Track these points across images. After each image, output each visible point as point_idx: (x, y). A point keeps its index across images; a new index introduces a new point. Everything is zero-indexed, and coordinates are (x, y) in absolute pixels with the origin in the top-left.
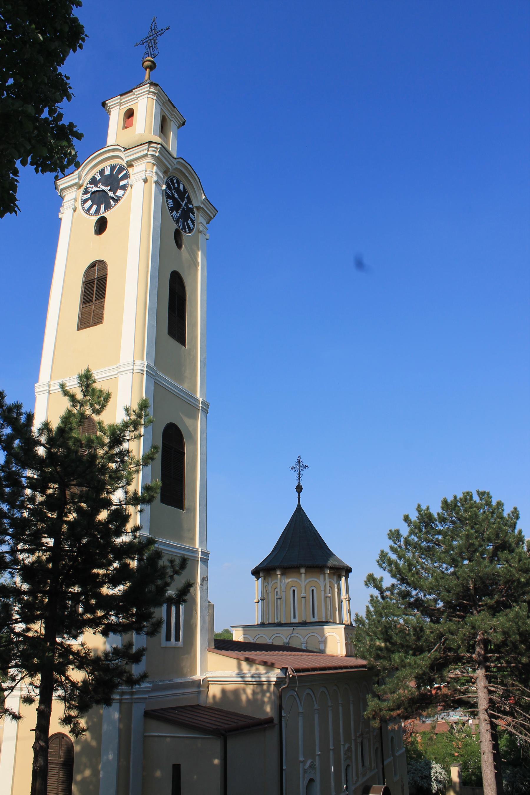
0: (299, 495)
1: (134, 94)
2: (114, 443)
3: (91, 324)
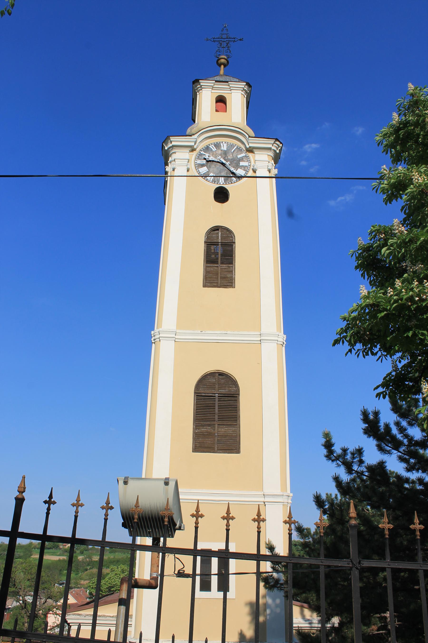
1: (229, 86)
3: (219, 285)
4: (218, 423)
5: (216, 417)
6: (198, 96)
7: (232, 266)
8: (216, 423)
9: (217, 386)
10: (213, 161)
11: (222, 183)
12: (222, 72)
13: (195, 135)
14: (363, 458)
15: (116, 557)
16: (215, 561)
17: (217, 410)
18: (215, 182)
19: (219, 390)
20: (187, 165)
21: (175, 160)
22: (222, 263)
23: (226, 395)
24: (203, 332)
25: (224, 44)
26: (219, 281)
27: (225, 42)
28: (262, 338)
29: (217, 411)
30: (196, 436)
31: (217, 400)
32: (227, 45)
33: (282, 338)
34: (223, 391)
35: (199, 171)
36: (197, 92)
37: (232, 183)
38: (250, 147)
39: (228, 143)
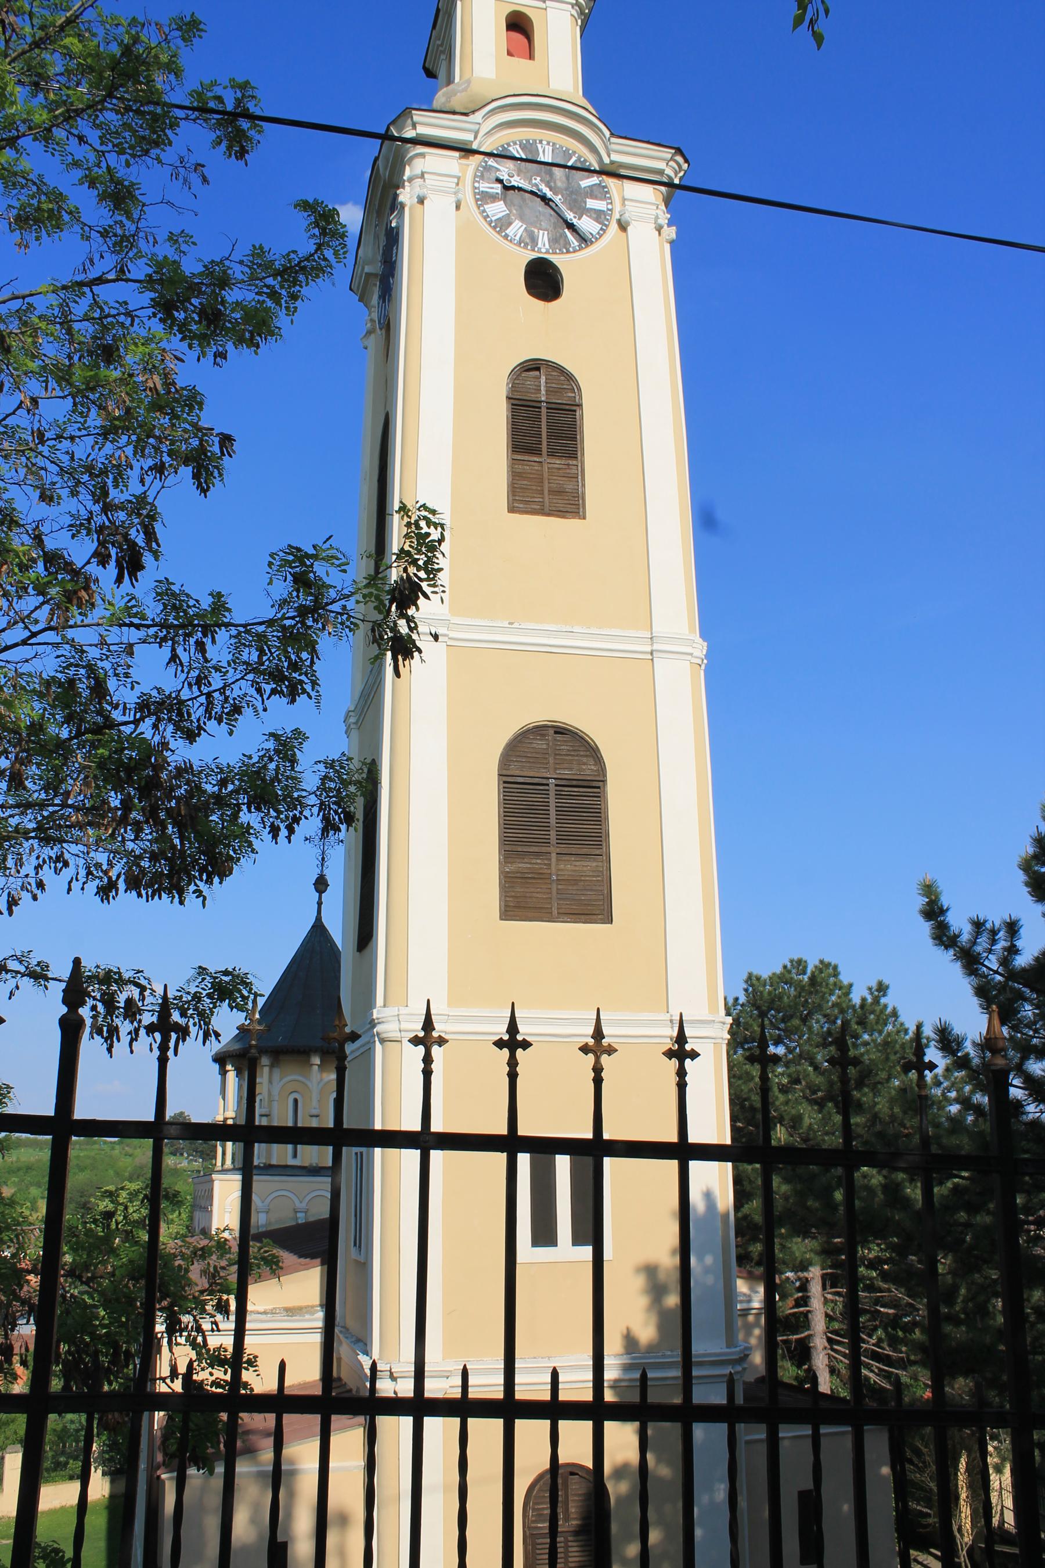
0: (320, 898)
2: (41, 725)
4: (558, 850)
5: (553, 834)
7: (575, 462)
8: (553, 850)
9: (551, 760)
10: (520, 189)
11: (543, 250)
13: (477, 114)
14: (1019, 944)
15: (23, 1159)
17: (554, 816)
18: (526, 245)
19: (556, 769)
20: (455, 193)
21: (423, 174)
22: (551, 454)
23: (574, 783)
24: (516, 625)
26: (547, 500)
28: (656, 647)
29: (553, 820)
30: (509, 882)
31: (552, 793)
33: (700, 648)
34: (566, 773)
35: (484, 211)
37: (568, 252)
38: (612, 163)
39: (554, 144)
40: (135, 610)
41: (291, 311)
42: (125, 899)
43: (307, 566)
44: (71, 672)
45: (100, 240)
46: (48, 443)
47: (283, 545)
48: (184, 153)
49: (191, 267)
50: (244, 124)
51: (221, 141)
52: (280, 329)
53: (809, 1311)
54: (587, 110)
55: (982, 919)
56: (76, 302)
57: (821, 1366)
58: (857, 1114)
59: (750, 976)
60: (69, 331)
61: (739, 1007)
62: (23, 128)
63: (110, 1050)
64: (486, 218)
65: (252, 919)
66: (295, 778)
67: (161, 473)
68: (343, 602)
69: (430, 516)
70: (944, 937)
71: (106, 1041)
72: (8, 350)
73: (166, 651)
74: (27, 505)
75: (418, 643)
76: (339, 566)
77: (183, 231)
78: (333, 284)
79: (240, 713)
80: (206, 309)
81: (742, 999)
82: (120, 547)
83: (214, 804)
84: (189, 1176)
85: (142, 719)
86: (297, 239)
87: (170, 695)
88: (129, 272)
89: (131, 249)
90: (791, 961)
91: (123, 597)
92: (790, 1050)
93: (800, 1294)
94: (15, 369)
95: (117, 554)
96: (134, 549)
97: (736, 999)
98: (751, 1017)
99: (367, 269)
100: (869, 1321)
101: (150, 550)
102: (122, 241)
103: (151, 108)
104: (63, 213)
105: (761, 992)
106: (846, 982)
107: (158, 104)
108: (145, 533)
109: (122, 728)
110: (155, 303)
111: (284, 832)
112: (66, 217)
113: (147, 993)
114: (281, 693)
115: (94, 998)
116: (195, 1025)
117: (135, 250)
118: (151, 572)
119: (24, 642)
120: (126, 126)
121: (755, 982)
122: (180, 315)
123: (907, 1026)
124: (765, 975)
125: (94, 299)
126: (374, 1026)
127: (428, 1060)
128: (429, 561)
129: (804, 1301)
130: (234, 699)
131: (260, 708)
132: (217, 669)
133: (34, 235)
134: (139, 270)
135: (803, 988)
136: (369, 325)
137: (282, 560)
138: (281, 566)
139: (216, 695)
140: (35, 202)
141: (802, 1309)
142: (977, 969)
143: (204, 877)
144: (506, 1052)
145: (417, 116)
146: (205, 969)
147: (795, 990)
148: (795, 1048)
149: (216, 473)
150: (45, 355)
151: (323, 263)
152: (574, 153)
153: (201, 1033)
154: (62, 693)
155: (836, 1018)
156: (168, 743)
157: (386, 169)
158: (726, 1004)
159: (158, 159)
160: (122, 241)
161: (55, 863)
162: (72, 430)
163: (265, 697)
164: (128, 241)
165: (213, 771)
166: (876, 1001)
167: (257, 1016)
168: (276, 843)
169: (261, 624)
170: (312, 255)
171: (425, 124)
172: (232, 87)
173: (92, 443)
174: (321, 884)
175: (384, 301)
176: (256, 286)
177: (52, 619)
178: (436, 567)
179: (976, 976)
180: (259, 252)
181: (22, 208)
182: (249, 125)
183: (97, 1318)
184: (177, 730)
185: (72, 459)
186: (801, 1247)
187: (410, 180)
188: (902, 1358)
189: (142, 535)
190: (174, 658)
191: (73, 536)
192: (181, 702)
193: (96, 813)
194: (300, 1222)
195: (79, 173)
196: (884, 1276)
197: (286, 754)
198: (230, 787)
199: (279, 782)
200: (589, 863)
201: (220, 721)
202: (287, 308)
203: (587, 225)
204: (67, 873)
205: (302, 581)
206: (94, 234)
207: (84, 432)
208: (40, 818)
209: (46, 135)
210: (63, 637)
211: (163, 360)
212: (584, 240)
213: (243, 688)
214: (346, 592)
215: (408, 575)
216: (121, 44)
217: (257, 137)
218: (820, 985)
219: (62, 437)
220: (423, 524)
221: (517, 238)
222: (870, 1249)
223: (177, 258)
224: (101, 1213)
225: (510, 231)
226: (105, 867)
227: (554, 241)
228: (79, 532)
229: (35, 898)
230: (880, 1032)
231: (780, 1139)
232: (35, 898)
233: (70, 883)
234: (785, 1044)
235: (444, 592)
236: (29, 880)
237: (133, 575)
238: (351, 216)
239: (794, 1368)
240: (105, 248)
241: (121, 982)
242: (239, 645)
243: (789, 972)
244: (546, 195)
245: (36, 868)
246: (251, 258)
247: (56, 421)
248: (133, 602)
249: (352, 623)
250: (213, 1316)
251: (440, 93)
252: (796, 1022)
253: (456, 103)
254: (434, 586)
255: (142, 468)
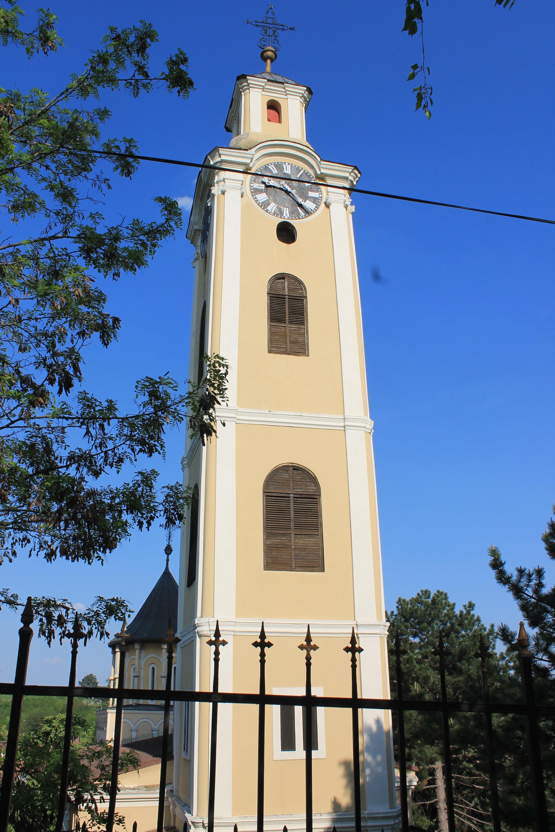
0: (168, 557)
1: (284, 89)
4: (295, 532)
5: (292, 524)
6: (243, 97)
7: (303, 327)
8: (292, 532)
10: (274, 187)
11: (286, 218)
12: (268, 69)
13: (252, 150)
14: (544, 581)
16: (298, 710)
17: (293, 514)
18: (277, 215)
19: (294, 489)
20: (241, 189)
21: (224, 179)
22: (291, 322)
23: (304, 496)
25: (270, 32)
26: (288, 347)
27: (271, 28)
28: (346, 423)
29: (292, 516)
30: (268, 549)
31: (292, 502)
32: (274, 34)
33: (370, 424)
34: (299, 491)
35: (256, 198)
36: (241, 92)
37: (299, 218)
38: (322, 174)
39: (292, 164)
40: (66, 410)
41: (152, 253)
42: (60, 560)
43: (156, 388)
44: (33, 440)
45: (55, 217)
46: (24, 321)
47: (144, 377)
48: (99, 173)
49: (101, 230)
50: (130, 160)
51: (118, 168)
52: (147, 261)
53: (436, 787)
54: (308, 147)
55: (523, 568)
56: (41, 249)
57: (444, 820)
58: (460, 675)
59: (400, 600)
60: (37, 264)
61: (394, 617)
62: (17, 163)
63: (49, 643)
64: (256, 201)
65: (129, 571)
66: (151, 496)
67: (83, 335)
68: (175, 406)
69: (221, 361)
70: (503, 578)
71: (47, 638)
72: (4, 276)
73: (84, 430)
74: (12, 352)
75: (215, 428)
76: (172, 388)
77: (97, 212)
78: (174, 239)
79: (123, 462)
80: (107, 251)
81: (396, 612)
82: (61, 375)
83: (108, 509)
84: (95, 710)
85: (71, 465)
86: (157, 216)
87: (85, 452)
88: (69, 232)
89: (71, 221)
90: (422, 591)
91: (59, 403)
92: (422, 640)
93: (431, 778)
94: (7, 284)
95: (59, 378)
96: (68, 376)
97: (392, 612)
98: (400, 622)
99: (195, 227)
100: (469, 793)
101: (77, 376)
102: (66, 217)
103: (83, 153)
104: (37, 203)
105: (406, 609)
106: (451, 603)
107: (85, 150)
108: (74, 368)
109: (60, 470)
110: (81, 249)
111: (145, 525)
112: (38, 206)
113: (70, 612)
114: (144, 451)
115: (41, 615)
116: (96, 628)
117: (73, 222)
118: (77, 387)
119: (8, 426)
120: (70, 161)
121: (402, 603)
122: (94, 255)
123: (485, 626)
124: (408, 599)
125: (51, 247)
126: (196, 628)
127: (217, 653)
128: (220, 384)
129: (433, 782)
130: (119, 454)
131: (133, 459)
132: (111, 438)
133: (21, 215)
134: (74, 232)
135: (428, 606)
136: (196, 256)
137: (143, 385)
138: (142, 388)
139: (110, 452)
140: (22, 198)
141: (432, 786)
142: (521, 596)
143: (102, 549)
144: (259, 649)
145: (221, 151)
146: (102, 598)
147: (424, 607)
148: (425, 639)
149: (112, 336)
150: (25, 275)
151: (169, 228)
152: (302, 169)
153: (99, 633)
154: (29, 451)
155: (447, 622)
156: (84, 478)
157: (205, 177)
158: (386, 615)
159: (86, 177)
160: (66, 217)
161: (22, 542)
162: (36, 315)
163: (136, 453)
164: (69, 217)
165: (107, 492)
166: (468, 612)
167: (126, 629)
168: (141, 531)
169: (131, 417)
170: (164, 224)
171: (226, 155)
172: (124, 141)
173: (46, 322)
174: (168, 550)
175: (204, 244)
176: (135, 240)
177: (22, 414)
178: (224, 387)
179: (521, 599)
180: (136, 222)
181: (16, 201)
182: (132, 160)
183: (36, 796)
184: (89, 471)
185: (36, 329)
186: (430, 751)
187: (218, 182)
188: (489, 815)
189: (72, 369)
190: (88, 433)
191: (36, 368)
192: (92, 456)
193: (44, 515)
194: (155, 736)
195: (45, 184)
196: (477, 767)
197: (147, 483)
198: (117, 501)
199: (143, 498)
200: (312, 539)
201: (112, 466)
202: (150, 251)
203: (309, 205)
204: (29, 546)
205: (154, 395)
206: (52, 214)
207: (43, 316)
208: (16, 516)
209: (28, 166)
210: (28, 424)
211: (83, 281)
212: (308, 212)
213: (124, 449)
214: (176, 401)
215: (209, 393)
216: (68, 122)
217: (136, 165)
218: (438, 604)
219: (31, 318)
220: (217, 365)
221: (273, 211)
222: (468, 752)
223: (94, 226)
224: (43, 733)
225: (269, 208)
226: (49, 543)
227: (291, 213)
228: (39, 366)
229: (11, 561)
230: (471, 630)
231: (416, 690)
232: (11, 561)
233: (31, 551)
234: (419, 637)
235: (228, 400)
236: (8, 550)
237: (67, 390)
238: (185, 203)
239: (429, 820)
240: (57, 221)
241: (56, 606)
242: (122, 427)
243: (421, 597)
244: (288, 190)
245: (12, 544)
246: (132, 226)
247: (28, 310)
248: (65, 406)
249: (179, 417)
250: (101, 794)
251: (233, 139)
252: (425, 624)
253: (241, 144)
254: (223, 397)
255: (72, 335)
